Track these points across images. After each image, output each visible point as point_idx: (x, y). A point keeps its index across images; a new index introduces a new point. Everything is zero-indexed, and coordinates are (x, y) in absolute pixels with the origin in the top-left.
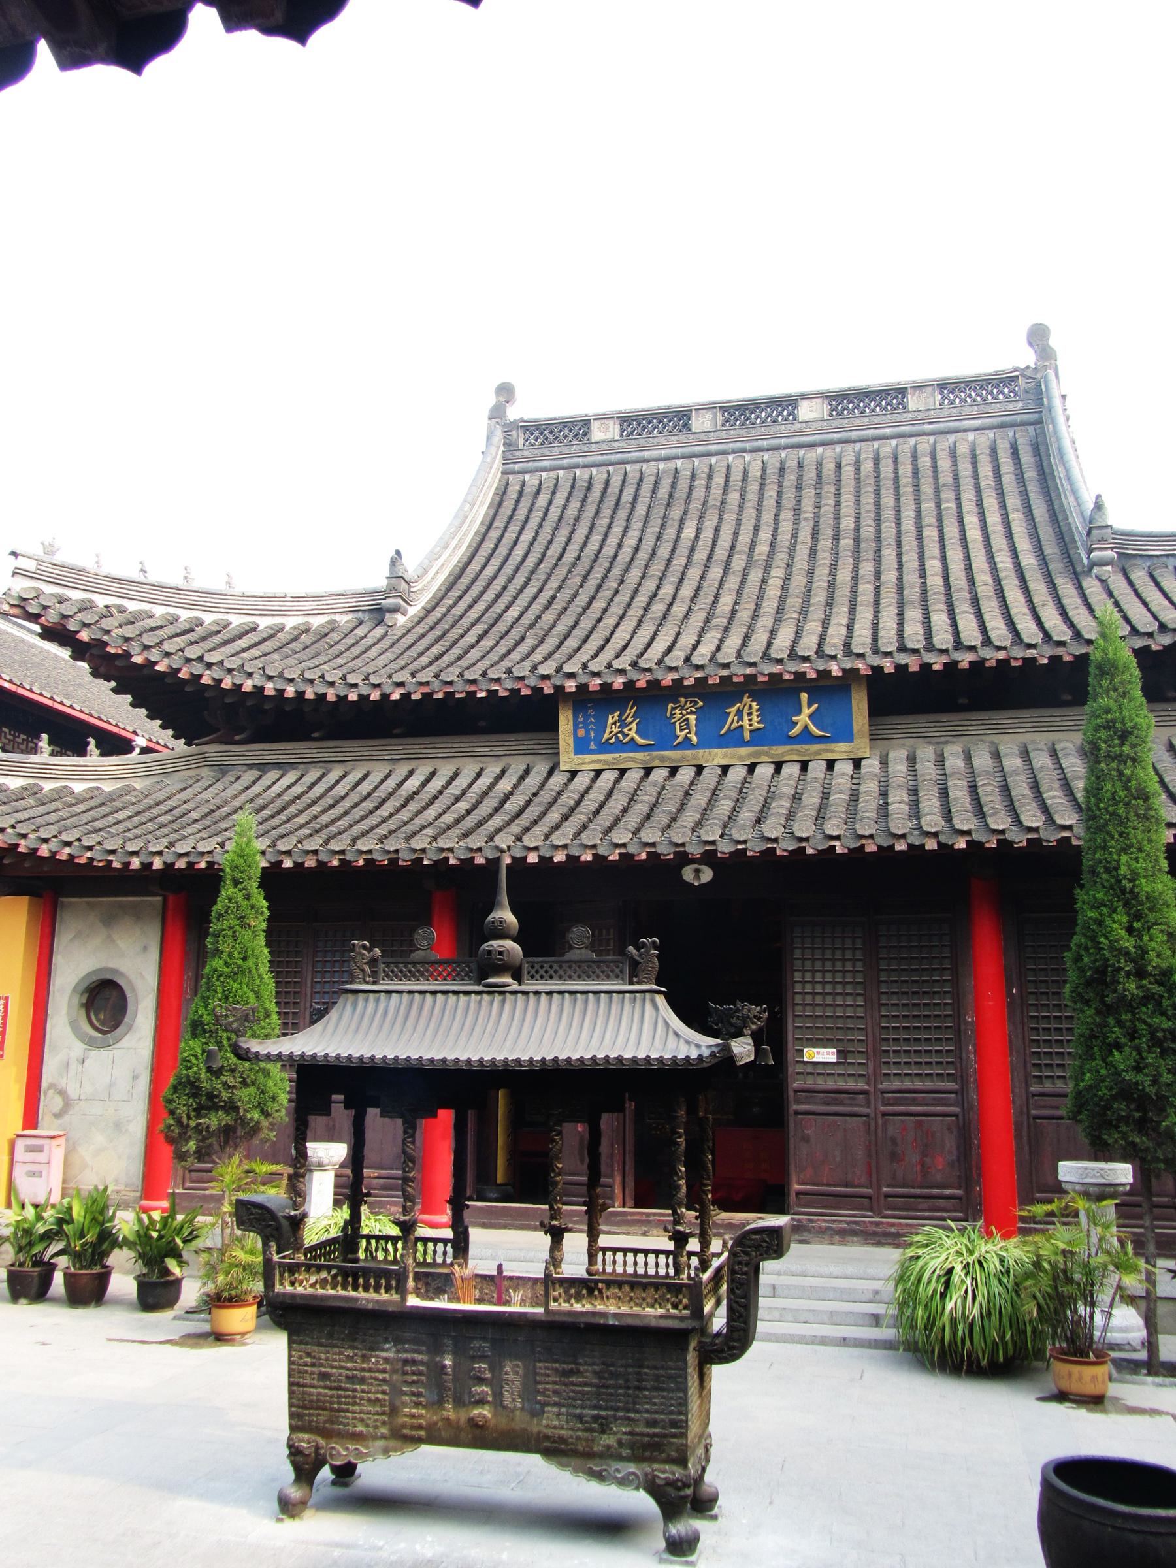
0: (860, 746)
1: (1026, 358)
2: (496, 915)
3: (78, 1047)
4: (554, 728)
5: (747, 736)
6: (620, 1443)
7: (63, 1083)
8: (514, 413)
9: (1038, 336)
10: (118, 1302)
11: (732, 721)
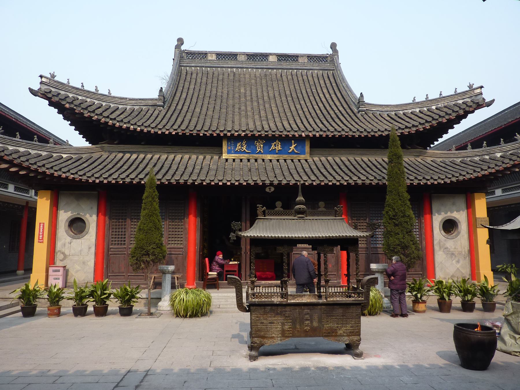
0: (307, 156)
1: (330, 52)
2: (298, 199)
3: (69, 239)
4: (221, 146)
5: (277, 152)
6: (344, 333)
7: (63, 250)
8: (183, 48)
9: (333, 46)
10: (65, 314)
11: (273, 147)
